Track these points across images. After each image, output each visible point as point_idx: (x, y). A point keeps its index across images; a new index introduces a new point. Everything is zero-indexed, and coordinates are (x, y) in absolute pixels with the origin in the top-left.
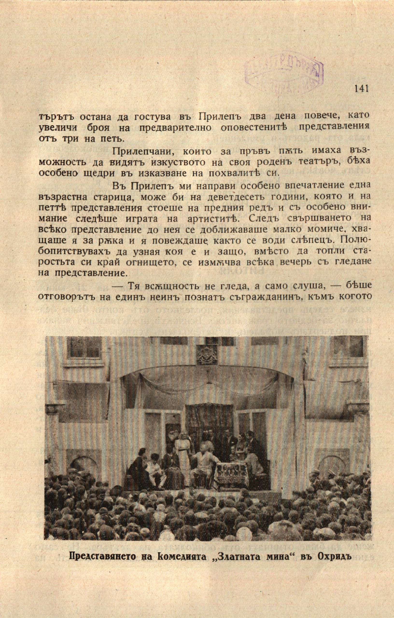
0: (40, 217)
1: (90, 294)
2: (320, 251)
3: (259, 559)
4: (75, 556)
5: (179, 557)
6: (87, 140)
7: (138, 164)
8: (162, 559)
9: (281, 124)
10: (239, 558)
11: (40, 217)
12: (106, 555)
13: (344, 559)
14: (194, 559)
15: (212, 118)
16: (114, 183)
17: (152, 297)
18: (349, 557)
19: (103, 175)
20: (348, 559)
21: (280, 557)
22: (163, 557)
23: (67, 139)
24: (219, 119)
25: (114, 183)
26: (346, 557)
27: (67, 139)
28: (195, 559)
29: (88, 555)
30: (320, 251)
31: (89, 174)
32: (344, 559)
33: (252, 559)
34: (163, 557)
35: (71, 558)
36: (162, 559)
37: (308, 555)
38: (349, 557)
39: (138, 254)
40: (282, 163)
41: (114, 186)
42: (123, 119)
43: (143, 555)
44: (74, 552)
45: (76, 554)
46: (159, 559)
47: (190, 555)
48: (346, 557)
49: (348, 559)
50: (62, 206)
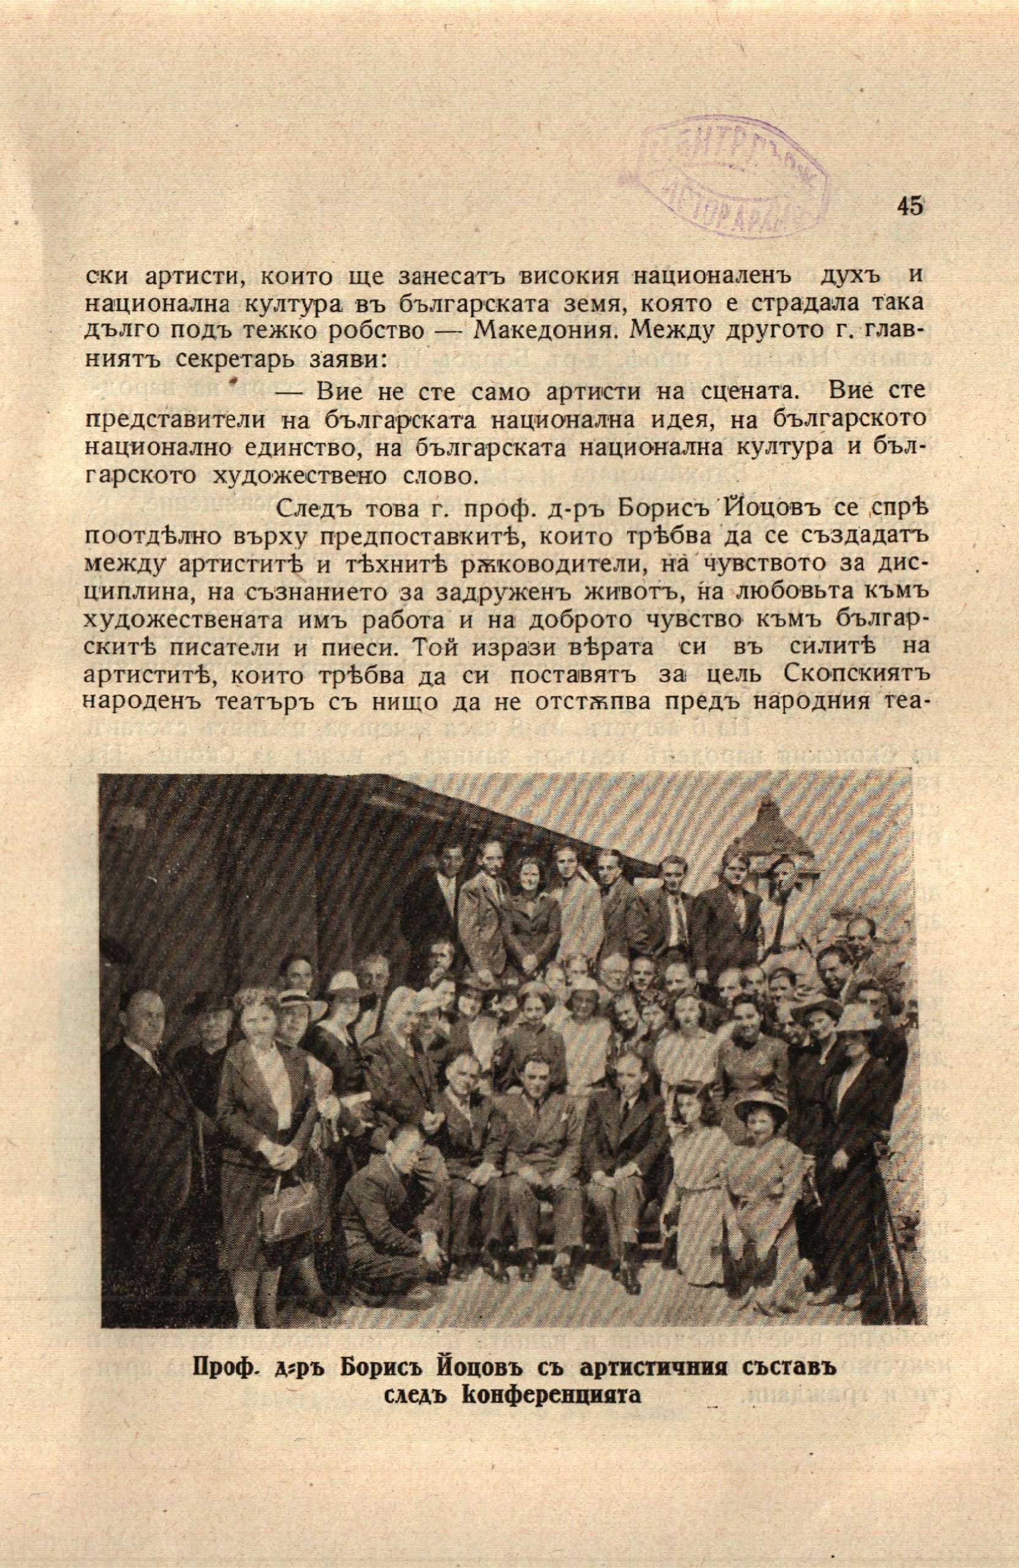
0: (88, 560)
1: (914, 527)
2: (376, 512)
3: (638, 1401)
4: (205, 1367)
5: (415, 1397)
6: (495, 624)
7: (914, 676)
8: (473, 1401)
9: (195, 668)
10: (618, 1370)
11: (88, 560)
12: (811, 1363)
13: (428, 1401)
14: (611, 1399)
15: (261, 680)
16: (832, 382)
17: (613, 277)
18: (831, 1370)
19: (740, 333)
20: (437, 1401)
21: (690, 1367)
22: (475, 1395)
23: (636, 538)
24: (820, 651)
25: (832, 382)
26: (432, 1397)
27: (636, 538)
28: (614, 1401)
29: (402, 1392)
30: (376, 512)
31: (363, 280)
32: (428, 1401)
33: (622, 1401)
34: (475, 1395)
35: (196, 1372)
36: (473, 1401)
37: (514, 1365)
38: (831, 1370)
39: (762, 453)
40: (177, 705)
41: (833, 388)
42: (818, 307)
43: (725, 1373)
44: (205, 1358)
45: (213, 1364)
46: (465, 1401)
47: (711, 1363)
48: (432, 1397)
49: (437, 1401)
50: (590, 643)
